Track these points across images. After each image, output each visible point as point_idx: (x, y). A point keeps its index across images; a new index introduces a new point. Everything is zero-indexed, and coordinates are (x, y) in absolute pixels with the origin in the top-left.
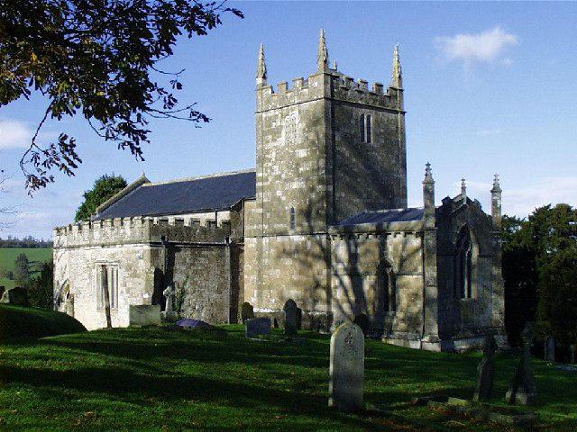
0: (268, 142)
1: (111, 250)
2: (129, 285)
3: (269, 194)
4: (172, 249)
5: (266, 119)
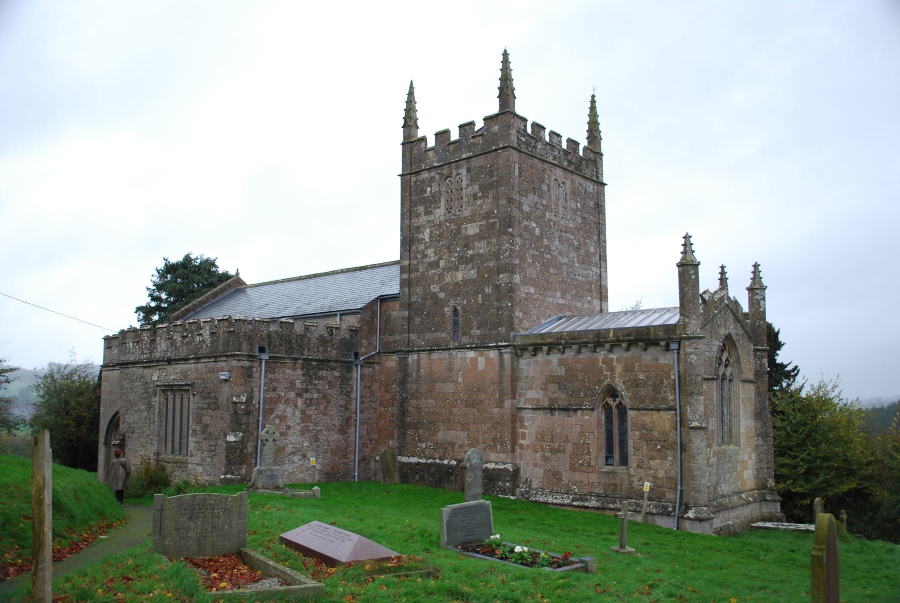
0: (418, 215)
1: (180, 367)
2: (206, 420)
4: (601, 311)
5: (415, 183)
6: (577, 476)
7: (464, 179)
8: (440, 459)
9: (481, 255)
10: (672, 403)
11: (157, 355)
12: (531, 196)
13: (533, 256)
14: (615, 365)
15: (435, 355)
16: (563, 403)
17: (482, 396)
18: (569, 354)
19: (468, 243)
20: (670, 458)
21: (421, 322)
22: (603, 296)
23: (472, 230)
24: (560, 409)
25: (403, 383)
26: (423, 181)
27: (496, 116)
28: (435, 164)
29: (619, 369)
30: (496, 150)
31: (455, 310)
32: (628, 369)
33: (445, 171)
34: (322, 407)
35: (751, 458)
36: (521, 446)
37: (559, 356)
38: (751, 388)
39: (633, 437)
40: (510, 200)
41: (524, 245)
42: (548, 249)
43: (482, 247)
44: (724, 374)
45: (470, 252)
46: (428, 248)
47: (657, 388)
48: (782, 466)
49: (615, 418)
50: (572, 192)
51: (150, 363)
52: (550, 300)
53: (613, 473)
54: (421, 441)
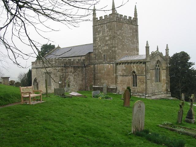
0: (96, 35)
4: (137, 54)
12: (119, 31)
14: (135, 68)
15: (100, 65)
16: (125, 75)
18: (126, 64)
22: (138, 50)
23: (107, 38)
25: (94, 71)
26: (97, 28)
27: (111, 14)
29: (135, 67)
31: (104, 55)
32: (137, 68)
33: (102, 25)
34: (78, 76)
36: (118, 83)
37: (124, 65)
38: (165, 71)
39: (138, 81)
40: (115, 33)
41: (118, 41)
42: (124, 42)
43: (109, 42)
44: (157, 68)
49: (135, 77)
52: (124, 53)
54: (98, 82)
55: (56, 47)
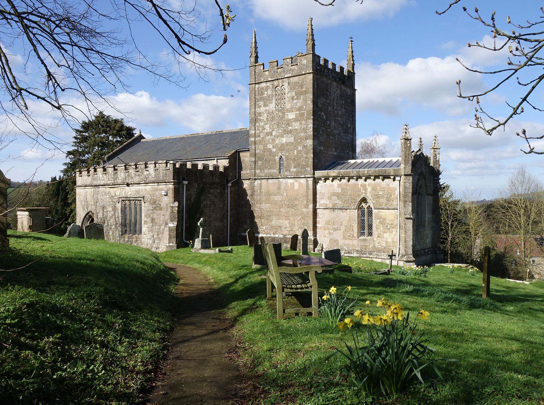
0: (260, 107)
3: (261, 147)
6: (347, 242)
7: (286, 89)
8: (274, 234)
9: (296, 130)
10: (396, 206)
11: (119, 181)
13: (322, 130)
17: (297, 203)
18: (344, 181)
19: (289, 123)
20: (394, 233)
21: (262, 164)
23: (291, 116)
24: (338, 209)
26: (262, 88)
28: (270, 79)
29: (369, 189)
30: (305, 74)
32: (374, 189)
33: (276, 83)
34: (212, 208)
35: (430, 233)
45: (290, 128)
46: (266, 124)
47: (388, 199)
48: (130, 230)
50: (341, 95)
51: (114, 185)
52: (330, 153)
53: (365, 240)
55: (137, 133)
